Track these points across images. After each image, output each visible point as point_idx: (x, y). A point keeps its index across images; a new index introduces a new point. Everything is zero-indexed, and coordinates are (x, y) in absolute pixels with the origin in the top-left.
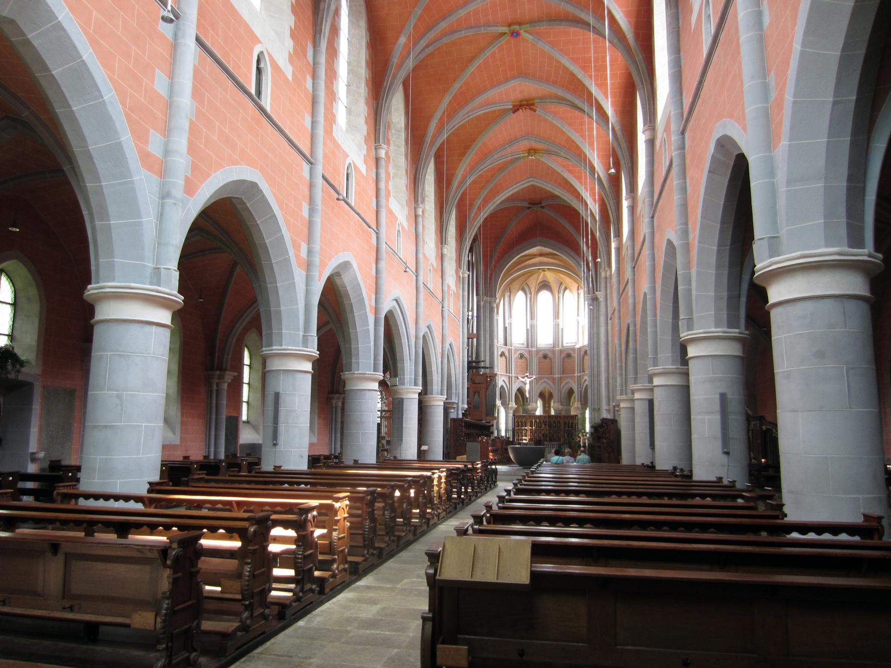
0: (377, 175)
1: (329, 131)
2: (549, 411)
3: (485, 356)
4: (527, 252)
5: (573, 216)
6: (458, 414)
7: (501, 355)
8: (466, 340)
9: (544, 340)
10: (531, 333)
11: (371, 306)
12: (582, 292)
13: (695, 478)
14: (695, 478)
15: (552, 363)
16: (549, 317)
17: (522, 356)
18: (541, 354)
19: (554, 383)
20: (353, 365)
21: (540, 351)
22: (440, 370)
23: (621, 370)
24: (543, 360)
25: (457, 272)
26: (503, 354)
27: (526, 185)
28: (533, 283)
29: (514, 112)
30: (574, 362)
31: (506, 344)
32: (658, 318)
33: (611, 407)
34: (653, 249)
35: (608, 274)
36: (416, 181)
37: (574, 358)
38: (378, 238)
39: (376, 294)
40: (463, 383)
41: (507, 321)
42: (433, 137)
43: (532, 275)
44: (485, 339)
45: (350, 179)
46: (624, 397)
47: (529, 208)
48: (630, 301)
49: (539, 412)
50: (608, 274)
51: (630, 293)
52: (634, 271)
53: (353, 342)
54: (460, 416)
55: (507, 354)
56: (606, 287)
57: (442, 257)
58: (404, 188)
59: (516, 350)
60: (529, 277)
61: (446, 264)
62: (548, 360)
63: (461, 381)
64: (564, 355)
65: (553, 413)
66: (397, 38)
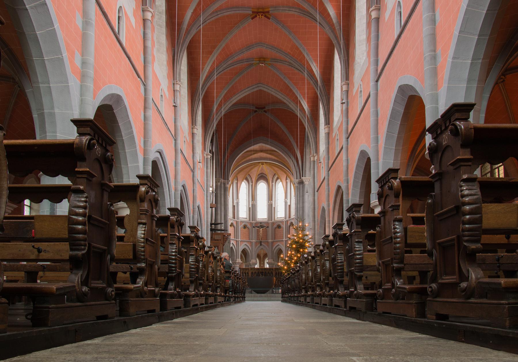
0: (145, 34)
4: (252, 148)
5: (290, 118)
7: (231, 226)
9: (262, 215)
10: (252, 210)
11: (140, 146)
12: (288, 181)
17: (245, 227)
19: (268, 246)
25: (203, 153)
26: (232, 225)
27: (255, 90)
28: (255, 173)
29: (252, 19)
30: (283, 230)
31: (234, 218)
35: (316, 158)
36: (174, 61)
37: (283, 228)
38: (145, 90)
39: (145, 137)
40: (207, 233)
41: (235, 201)
43: (255, 167)
44: (221, 209)
45: (121, 23)
47: (256, 111)
48: (344, 164)
50: (316, 158)
51: (344, 158)
55: (235, 225)
56: (314, 168)
57: (193, 135)
58: (165, 63)
59: (242, 222)
60: (252, 169)
64: (275, 226)
65: (267, 266)
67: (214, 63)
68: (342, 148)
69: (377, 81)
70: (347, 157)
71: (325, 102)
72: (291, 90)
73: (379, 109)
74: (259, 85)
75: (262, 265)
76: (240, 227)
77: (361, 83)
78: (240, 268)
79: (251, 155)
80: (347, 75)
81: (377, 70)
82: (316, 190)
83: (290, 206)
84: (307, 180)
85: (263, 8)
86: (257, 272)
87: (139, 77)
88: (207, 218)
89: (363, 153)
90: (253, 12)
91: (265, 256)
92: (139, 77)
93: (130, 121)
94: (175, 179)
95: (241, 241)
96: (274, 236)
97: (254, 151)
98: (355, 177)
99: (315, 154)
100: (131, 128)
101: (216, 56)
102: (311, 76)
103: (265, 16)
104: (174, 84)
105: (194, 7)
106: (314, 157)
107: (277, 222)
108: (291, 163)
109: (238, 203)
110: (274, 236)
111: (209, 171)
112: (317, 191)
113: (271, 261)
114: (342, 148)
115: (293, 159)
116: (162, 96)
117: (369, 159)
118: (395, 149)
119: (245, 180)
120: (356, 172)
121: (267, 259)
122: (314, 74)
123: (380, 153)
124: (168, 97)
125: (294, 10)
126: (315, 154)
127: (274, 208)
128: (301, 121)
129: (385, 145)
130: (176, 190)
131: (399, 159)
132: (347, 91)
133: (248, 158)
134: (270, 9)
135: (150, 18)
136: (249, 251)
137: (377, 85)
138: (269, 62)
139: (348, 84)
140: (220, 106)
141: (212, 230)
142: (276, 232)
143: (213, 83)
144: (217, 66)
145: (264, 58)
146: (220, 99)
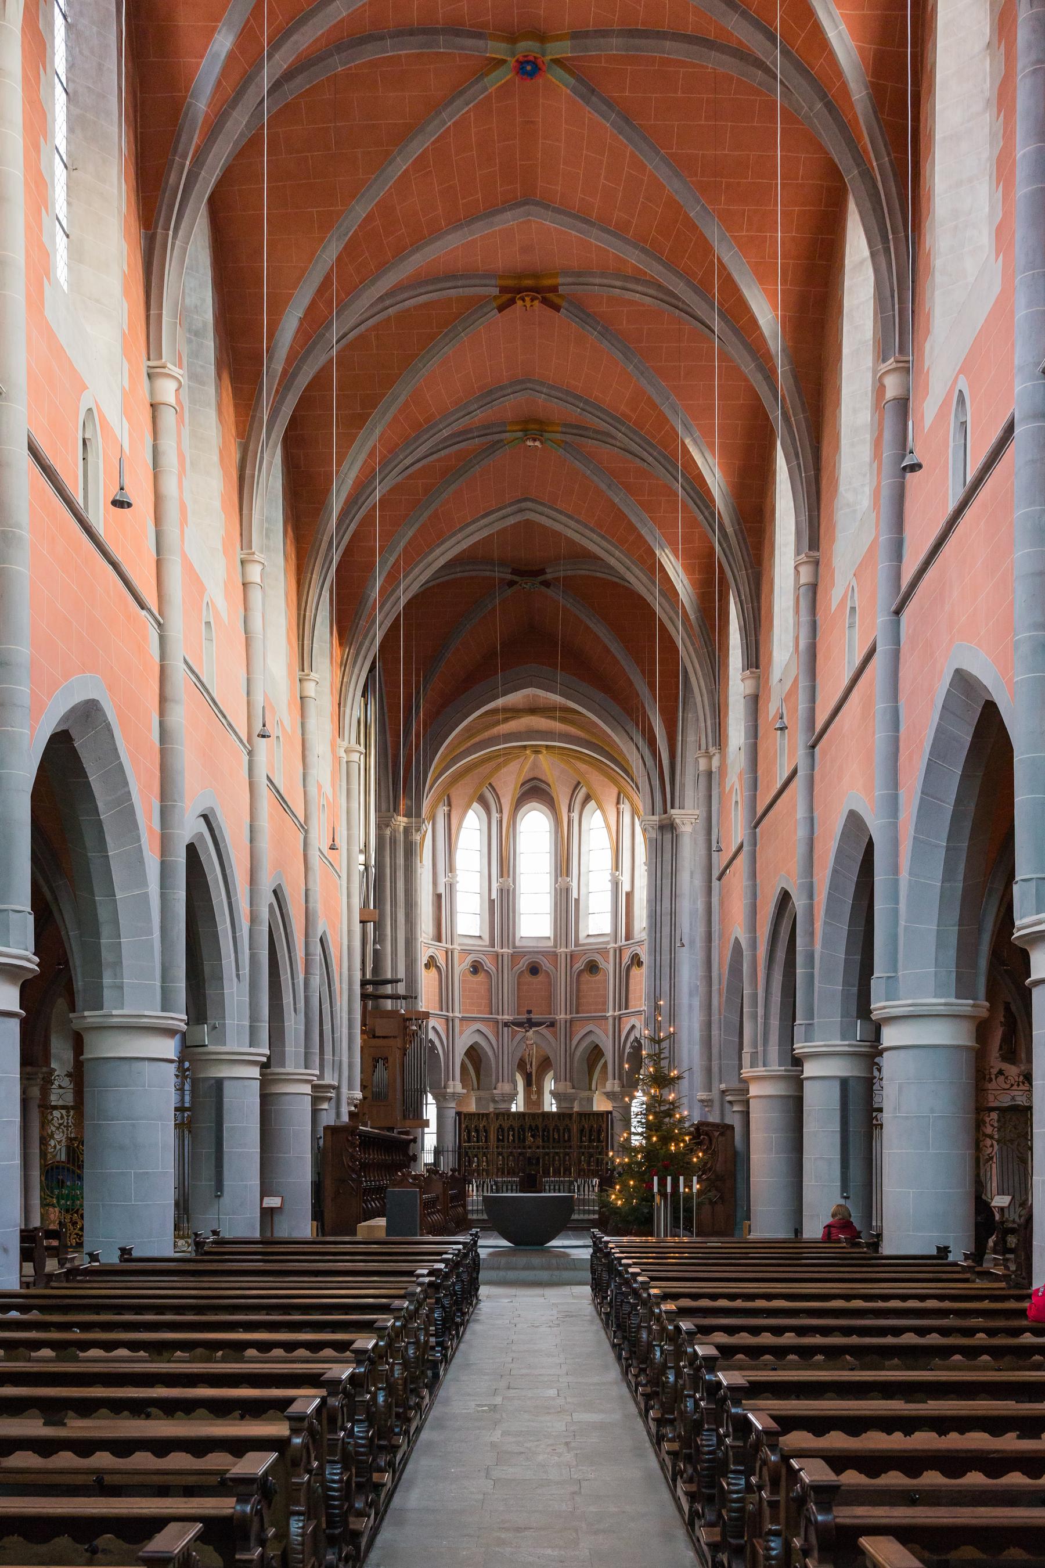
1: (36, 302)
2: (540, 1101)
3: (394, 968)
4: (500, 702)
5: (631, 615)
6: (338, 1114)
7: (427, 966)
8: (357, 927)
9: (535, 923)
10: (502, 907)
11: (150, 829)
12: (626, 807)
13: (888, 1248)
14: (888, 1248)
15: (544, 988)
16: (547, 869)
17: (476, 968)
18: (523, 964)
20: (106, 993)
21: (524, 954)
22: (301, 1005)
23: (755, 1004)
24: (528, 978)
26: (431, 963)
27: (511, 521)
28: (509, 781)
29: (501, 309)
32: (904, 875)
33: (715, 1094)
34: (895, 697)
38: (162, 639)
41: (442, 880)
42: (289, 360)
43: (506, 763)
46: (760, 1071)
47: (511, 584)
49: (517, 1106)
50: (715, 762)
52: (812, 756)
53: (105, 931)
54: (345, 1118)
55: (441, 961)
58: (217, 504)
60: (498, 767)
61: (312, 723)
62: (541, 978)
63: (345, 1031)
64: (579, 965)
65: (551, 1105)
66: (209, 33)
67: (372, 454)
68: (794, 773)
69: (898, 612)
70: (811, 809)
71: (745, 589)
72: (632, 528)
73: (902, 703)
74: (524, 505)
75: (534, 1097)
76: (461, 966)
77: (854, 583)
78: (458, 1114)
79: (498, 723)
80: (814, 535)
81: (899, 587)
82: (716, 874)
83: (629, 895)
84: (688, 818)
85: (536, 276)
86: (516, 1125)
87: (142, 606)
88: (350, 969)
89: (854, 820)
90: (504, 290)
91: (545, 1064)
92: (142, 606)
93: (121, 765)
94: (251, 884)
95: (462, 1019)
96: (577, 1003)
97: (505, 710)
98: (834, 886)
99: (712, 750)
100: (126, 783)
101: (377, 432)
102: (697, 493)
103: (545, 301)
104: (243, 562)
105: (306, 302)
106: (710, 758)
107: (585, 952)
108: (632, 754)
109: (451, 887)
110: (577, 1003)
111: (355, 786)
112: (719, 879)
113: (566, 1087)
114: (794, 773)
115: (641, 743)
116: (208, 623)
117: (870, 844)
118: (948, 849)
119: (475, 805)
120: (835, 871)
121: (551, 1074)
122: (708, 492)
123: (901, 848)
124: (225, 619)
125: (640, 288)
126: (712, 750)
127: (577, 901)
128: (663, 628)
129: (916, 830)
130: (254, 919)
131: (961, 877)
132: (814, 587)
133: (487, 734)
134: (561, 280)
135: (172, 400)
136: (490, 1053)
137: (896, 626)
138: (558, 436)
139: (817, 563)
140: (392, 580)
141: (364, 997)
142: (584, 987)
143: (381, 609)
144: (383, 465)
145: (540, 422)
146: (392, 560)
